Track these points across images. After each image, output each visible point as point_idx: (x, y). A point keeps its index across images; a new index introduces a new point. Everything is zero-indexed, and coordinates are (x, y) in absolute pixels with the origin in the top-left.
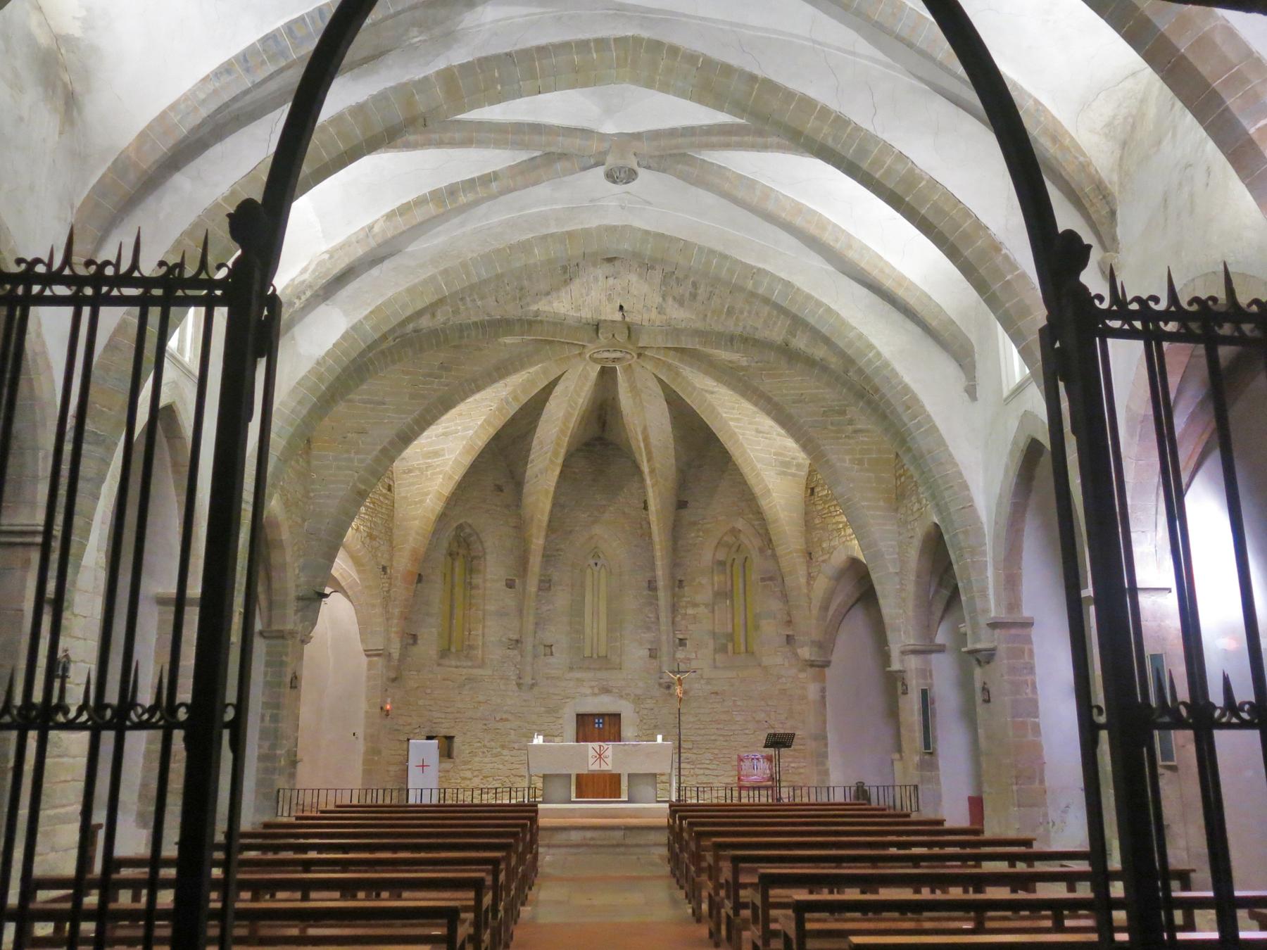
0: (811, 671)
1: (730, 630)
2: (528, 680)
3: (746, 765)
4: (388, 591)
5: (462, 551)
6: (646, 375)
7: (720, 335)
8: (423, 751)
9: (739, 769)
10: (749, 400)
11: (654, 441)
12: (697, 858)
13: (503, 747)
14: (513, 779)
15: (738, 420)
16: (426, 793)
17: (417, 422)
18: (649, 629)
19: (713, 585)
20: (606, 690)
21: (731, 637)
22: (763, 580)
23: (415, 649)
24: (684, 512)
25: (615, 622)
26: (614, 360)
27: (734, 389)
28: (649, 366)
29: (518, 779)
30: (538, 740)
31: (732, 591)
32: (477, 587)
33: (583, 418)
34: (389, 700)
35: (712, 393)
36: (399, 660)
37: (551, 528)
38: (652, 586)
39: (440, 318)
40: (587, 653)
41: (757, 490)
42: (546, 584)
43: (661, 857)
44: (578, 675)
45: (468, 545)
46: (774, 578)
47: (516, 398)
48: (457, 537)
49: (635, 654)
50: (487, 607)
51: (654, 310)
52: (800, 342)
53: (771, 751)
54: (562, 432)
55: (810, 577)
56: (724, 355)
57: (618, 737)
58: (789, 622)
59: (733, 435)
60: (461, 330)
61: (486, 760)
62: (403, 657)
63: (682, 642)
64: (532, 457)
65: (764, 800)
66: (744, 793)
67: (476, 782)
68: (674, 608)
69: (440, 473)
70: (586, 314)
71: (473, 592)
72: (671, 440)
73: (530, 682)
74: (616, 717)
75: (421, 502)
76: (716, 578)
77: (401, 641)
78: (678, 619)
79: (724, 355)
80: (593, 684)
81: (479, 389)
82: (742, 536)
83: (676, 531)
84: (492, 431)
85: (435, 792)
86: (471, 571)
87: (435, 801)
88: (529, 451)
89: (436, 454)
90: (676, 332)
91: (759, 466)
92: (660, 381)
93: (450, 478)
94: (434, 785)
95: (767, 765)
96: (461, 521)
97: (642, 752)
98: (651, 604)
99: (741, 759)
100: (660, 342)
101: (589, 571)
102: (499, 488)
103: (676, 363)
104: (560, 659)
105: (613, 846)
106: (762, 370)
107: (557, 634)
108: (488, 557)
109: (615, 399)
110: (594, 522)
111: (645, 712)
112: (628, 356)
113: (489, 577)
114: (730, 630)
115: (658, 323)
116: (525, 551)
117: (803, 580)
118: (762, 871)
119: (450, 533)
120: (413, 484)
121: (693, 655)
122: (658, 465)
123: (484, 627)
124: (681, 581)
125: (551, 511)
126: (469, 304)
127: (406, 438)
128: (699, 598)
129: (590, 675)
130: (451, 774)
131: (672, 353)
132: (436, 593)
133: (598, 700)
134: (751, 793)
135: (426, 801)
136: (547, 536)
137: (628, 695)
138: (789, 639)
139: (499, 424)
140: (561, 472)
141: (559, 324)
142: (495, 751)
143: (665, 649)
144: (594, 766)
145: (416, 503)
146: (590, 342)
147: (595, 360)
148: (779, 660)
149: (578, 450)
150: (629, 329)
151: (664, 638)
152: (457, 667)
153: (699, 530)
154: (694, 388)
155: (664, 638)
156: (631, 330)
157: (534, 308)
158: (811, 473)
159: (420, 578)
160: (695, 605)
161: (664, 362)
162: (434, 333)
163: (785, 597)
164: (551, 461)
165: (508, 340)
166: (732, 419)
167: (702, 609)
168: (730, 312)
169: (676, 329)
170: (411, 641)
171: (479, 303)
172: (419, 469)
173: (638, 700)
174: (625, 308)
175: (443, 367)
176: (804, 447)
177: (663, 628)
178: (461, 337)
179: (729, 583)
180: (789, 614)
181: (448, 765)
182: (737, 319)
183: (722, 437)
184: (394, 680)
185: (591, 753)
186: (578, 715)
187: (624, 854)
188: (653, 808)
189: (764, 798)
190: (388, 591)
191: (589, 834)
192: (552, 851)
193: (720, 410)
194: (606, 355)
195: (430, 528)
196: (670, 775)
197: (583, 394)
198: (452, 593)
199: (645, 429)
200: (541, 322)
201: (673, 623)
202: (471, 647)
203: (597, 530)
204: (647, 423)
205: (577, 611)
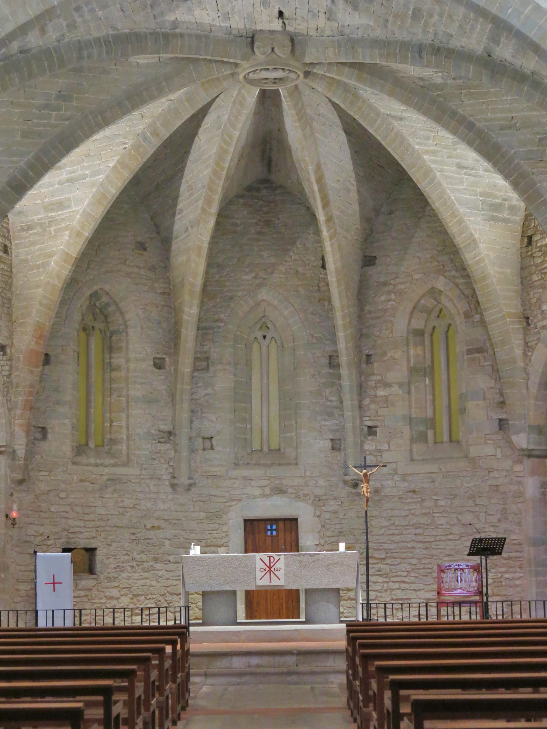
0: (528, 463)
1: (430, 414)
2: (184, 480)
3: (448, 576)
4: (9, 376)
5: (99, 325)
6: (317, 99)
7: (405, 46)
8: (54, 564)
9: (440, 581)
10: (446, 127)
11: (330, 181)
12: (366, 686)
13: (156, 560)
14: (169, 598)
15: (434, 153)
16: (59, 615)
17: (31, 166)
18: (330, 415)
19: (409, 361)
20: (279, 491)
21: (432, 423)
22: (469, 352)
23: (44, 445)
24: (371, 270)
25: (289, 406)
26: (276, 81)
27: (426, 113)
28: (320, 87)
29: (176, 598)
30: (196, 551)
31: (432, 367)
32: (118, 368)
33: (241, 156)
34: (15, 507)
35: (401, 119)
36: (26, 459)
37: (207, 292)
38: (333, 362)
39: (52, 34)
40: (256, 446)
41: (460, 241)
42: (203, 363)
43: (340, 685)
44: (244, 472)
45: (106, 317)
46: (482, 350)
47: (155, 133)
48: (92, 307)
49: (314, 446)
50: (131, 393)
51: (322, 15)
52: (505, 51)
53: (476, 559)
54: (215, 173)
55: (527, 347)
56: (413, 71)
57: (295, 546)
58: (502, 403)
59: (428, 172)
60: (80, 50)
61: (136, 575)
62: (30, 454)
63: (372, 430)
64: (179, 207)
65: (465, 617)
66: (443, 611)
67: (125, 601)
68: (361, 389)
69: (66, 228)
70: (237, 23)
71: (114, 374)
72: (353, 180)
73: (187, 482)
74: (292, 523)
75: (45, 265)
76: (412, 352)
77: (27, 436)
78: (367, 401)
79: (413, 71)
80: (263, 483)
81: (107, 123)
82: (443, 299)
83: (362, 293)
84: (127, 175)
85: (69, 614)
86: (111, 349)
87: (69, 624)
88: (176, 198)
89: (60, 205)
90: (350, 43)
91: (462, 210)
92: (336, 106)
93: (79, 234)
94: (69, 605)
95: (474, 576)
96: (95, 288)
97: (325, 563)
98: (333, 384)
99: (442, 570)
100: (332, 56)
101: (255, 346)
102: (142, 246)
103: (353, 83)
104: (223, 454)
105: (282, 674)
106: (460, 88)
107: (218, 423)
108: (131, 331)
109: (281, 129)
110: (259, 286)
111: (327, 516)
112: (292, 76)
113: (132, 355)
114: (430, 414)
115: (328, 32)
116: (176, 323)
117: (519, 352)
118: (414, 697)
119: (81, 302)
120: (33, 244)
121: (385, 447)
122: (336, 213)
123: (128, 417)
124: (369, 356)
125: (207, 273)
126: (88, 16)
127: (20, 186)
128: (391, 376)
129: (259, 472)
130: (94, 592)
131: (347, 70)
132: (68, 374)
133: (269, 502)
134: (473, 609)
135: (59, 624)
136: (202, 303)
137: (305, 495)
138: (502, 424)
139: (136, 165)
140: (218, 224)
141: (203, 37)
142: (146, 565)
143: (350, 439)
144: (263, 581)
145: (38, 267)
146: (243, 59)
147: (252, 82)
148: (489, 450)
149: (239, 196)
150: (292, 40)
151: (349, 425)
152: (97, 465)
153: (389, 293)
154: (378, 114)
155: (349, 425)
156: (294, 42)
157: (171, 17)
158: (527, 218)
159: (47, 359)
160: (387, 385)
161: (339, 82)
162: (46, 53)
163: (496, 372)
164: (203, 210)
165: (141, 59)
166: (427, 152)
167: (395, 390)
168: (417, 14)
169: (350, 39)
170: (39, 436)
171: (100, 13)
172: (41, 225)
173: (318, 501)
174: (286, 14)
175: (60, 96)
176: (515, 185)
177: (348, 414)
178: (80, 58)
179: (428, 356)
180: (501, 394)
181: (88, 582)
182: (426, 24)
183: (415, 175)
184: (21, 482)
185: (259, 565)
186: (246, 521)
187: (296, 683)
188: (330, 630)
189: (465, 615)
190: (9, 376)
191: (255, 661)
192: (210, 681)
193: (411, 140)
194: (264, 75)
195: (57, 297)
196: (356, 590)
197: (240, 125)
198: (88, 377)
199: (318, 168)
200: (181, 35)
201: (360, 407)
202: (113, 441)
203: (264, 295)
204: (322, 161)
205: (242, 395)
